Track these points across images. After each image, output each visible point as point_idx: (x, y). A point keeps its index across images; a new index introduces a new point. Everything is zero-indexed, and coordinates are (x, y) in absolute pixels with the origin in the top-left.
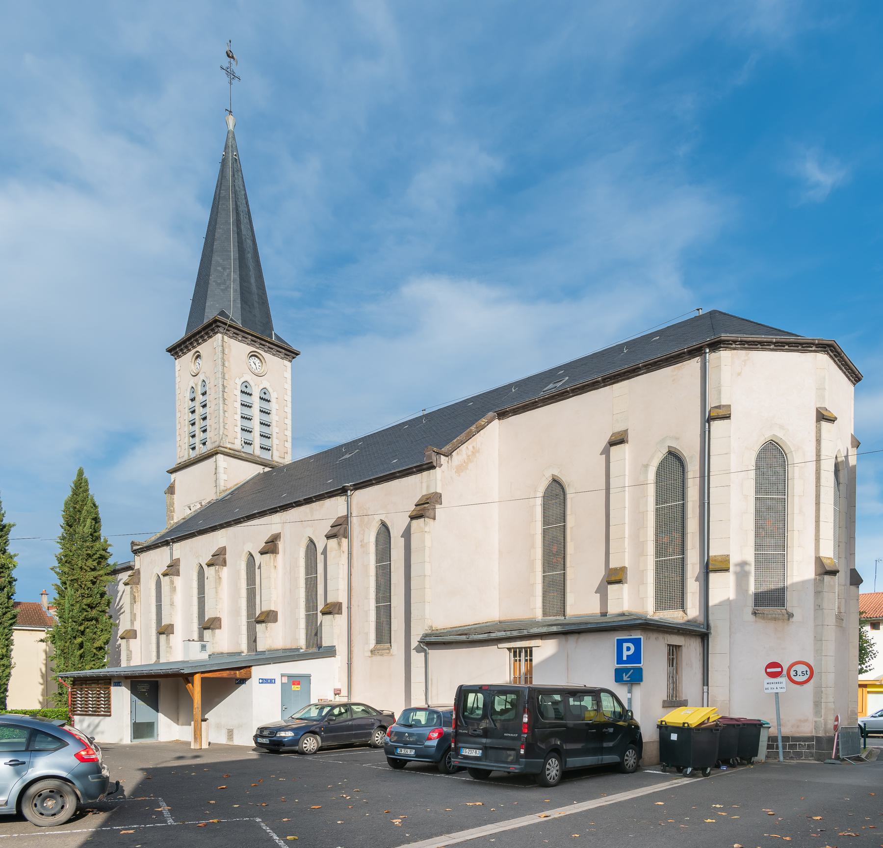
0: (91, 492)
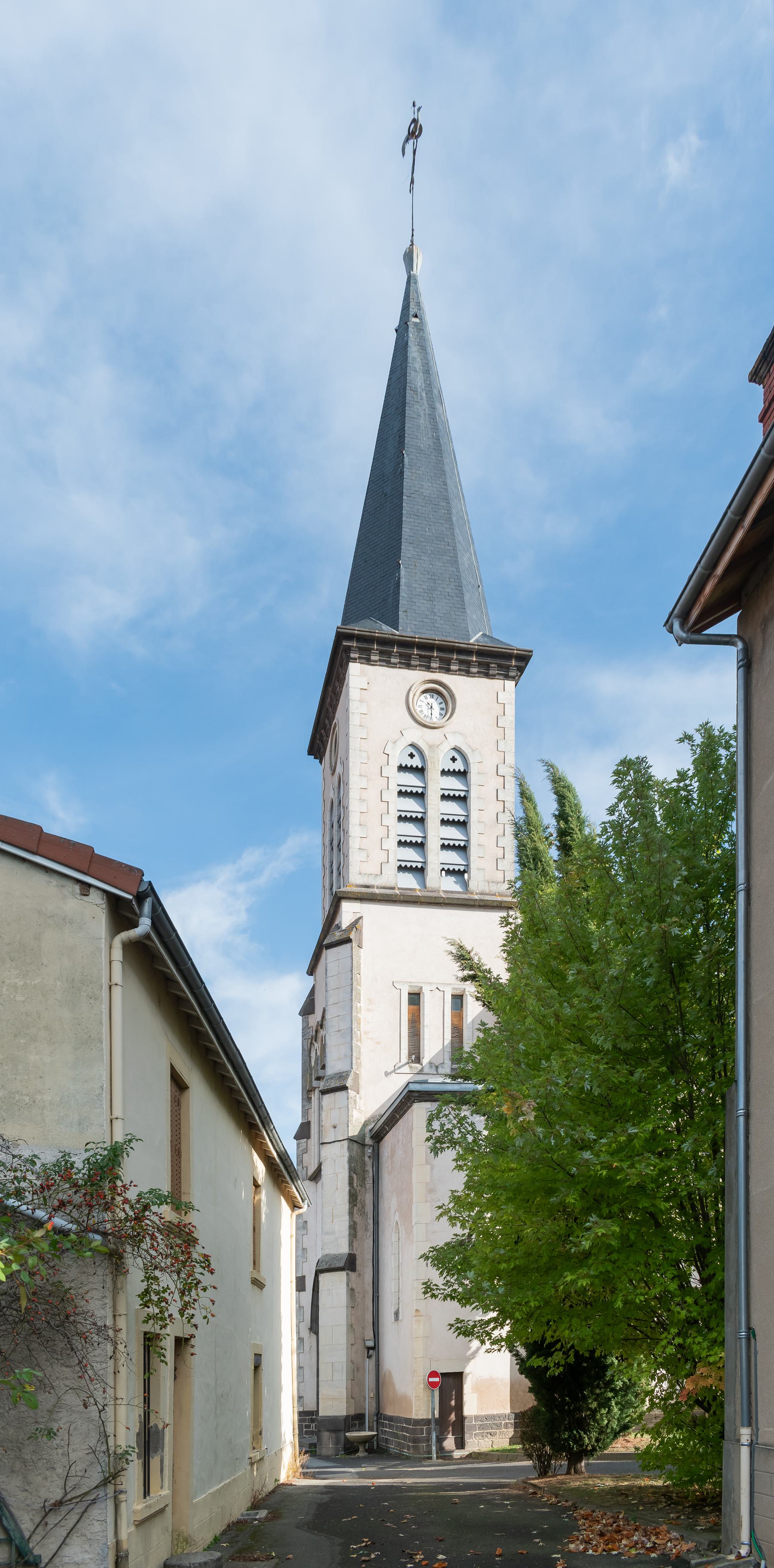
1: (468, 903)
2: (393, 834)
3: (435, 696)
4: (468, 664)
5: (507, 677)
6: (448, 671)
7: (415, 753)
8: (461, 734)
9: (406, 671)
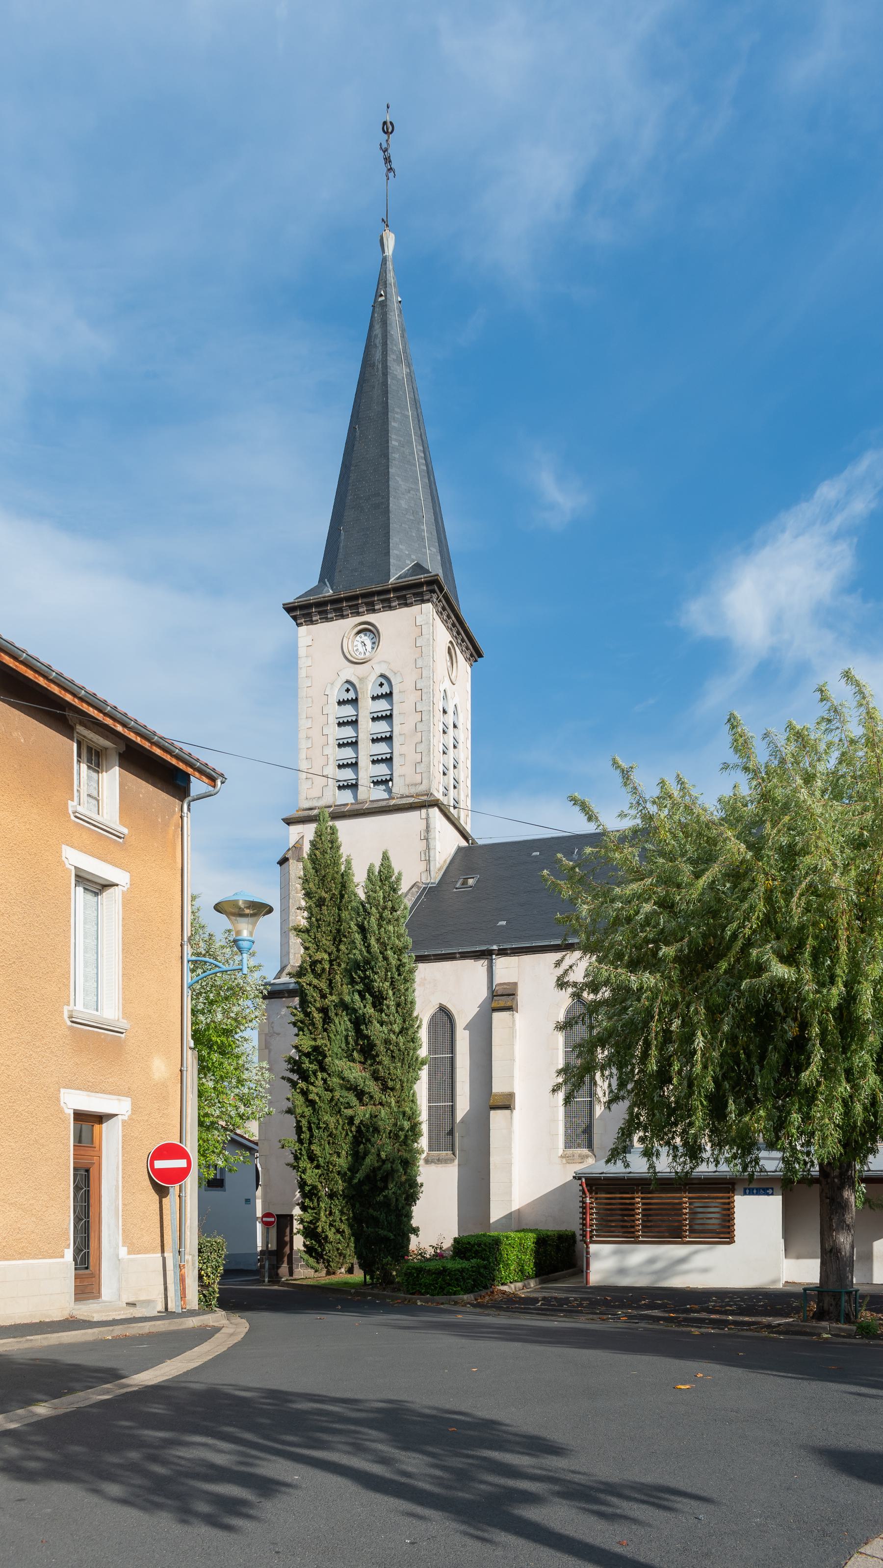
0: (344, 851)
1: (384, 809)
2: (331, 761)
3: (368, 633)
4: (388, 600)
5: (423, 601)
6: (374, 611)
7: (350, 688)
8: (385, 662)
9: (342, 621)
